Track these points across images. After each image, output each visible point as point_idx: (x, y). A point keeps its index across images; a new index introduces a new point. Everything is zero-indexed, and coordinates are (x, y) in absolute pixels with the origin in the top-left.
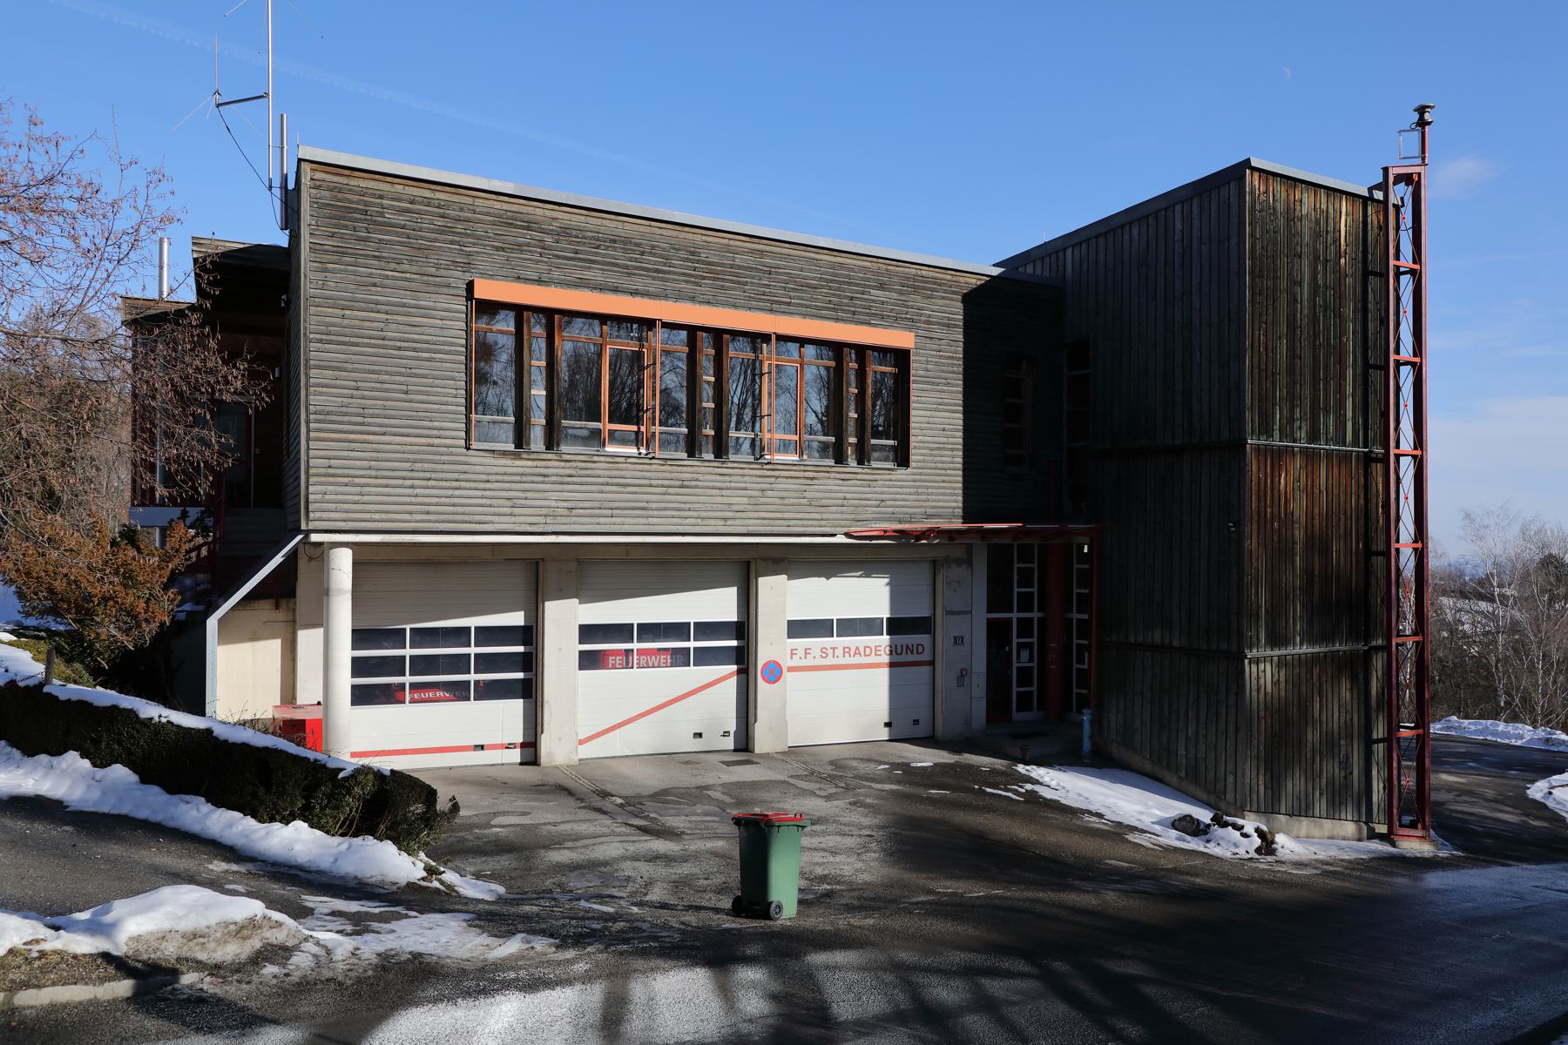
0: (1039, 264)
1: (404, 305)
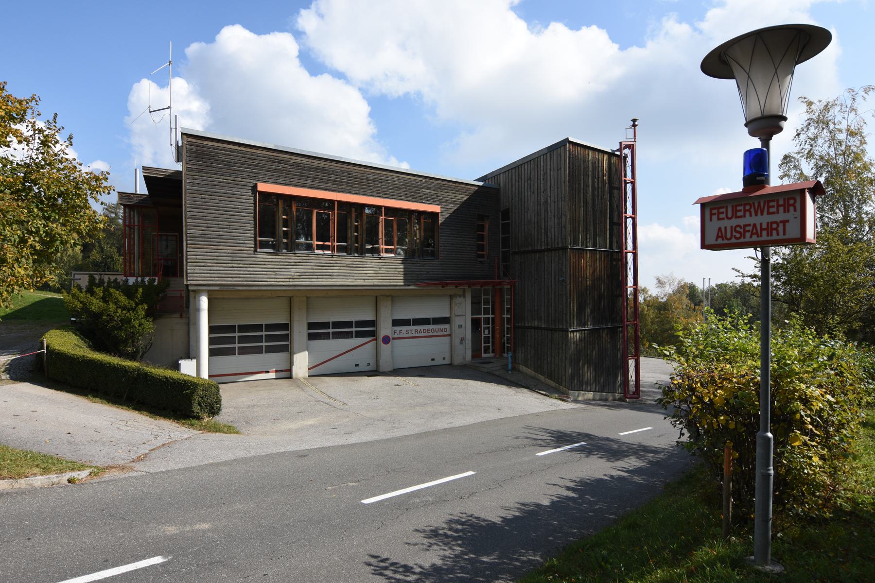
0: (490, 180)
1: (228, 194)
